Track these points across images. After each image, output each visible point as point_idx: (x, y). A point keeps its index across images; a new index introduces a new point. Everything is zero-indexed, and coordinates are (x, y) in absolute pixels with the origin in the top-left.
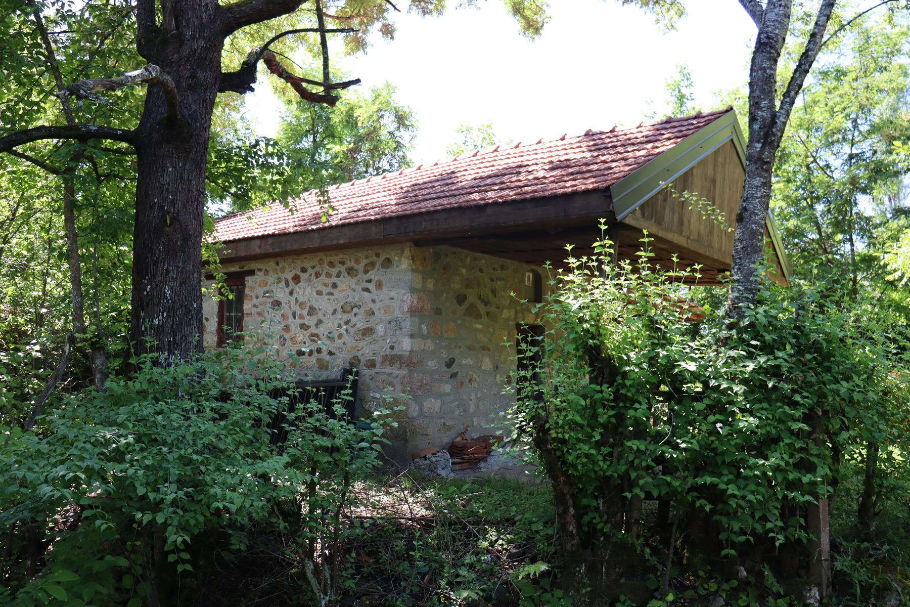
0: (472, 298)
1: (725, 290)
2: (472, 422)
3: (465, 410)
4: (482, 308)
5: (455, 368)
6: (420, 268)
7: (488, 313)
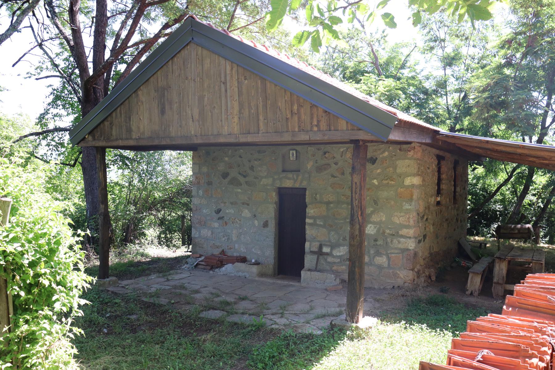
0: (233, 173)
1: (263, 320)
2: (235, 246)
3: (228, 239)
4: (242, 179)
5: (221, 214)
6: (198, 162)
7: (246, 182)
